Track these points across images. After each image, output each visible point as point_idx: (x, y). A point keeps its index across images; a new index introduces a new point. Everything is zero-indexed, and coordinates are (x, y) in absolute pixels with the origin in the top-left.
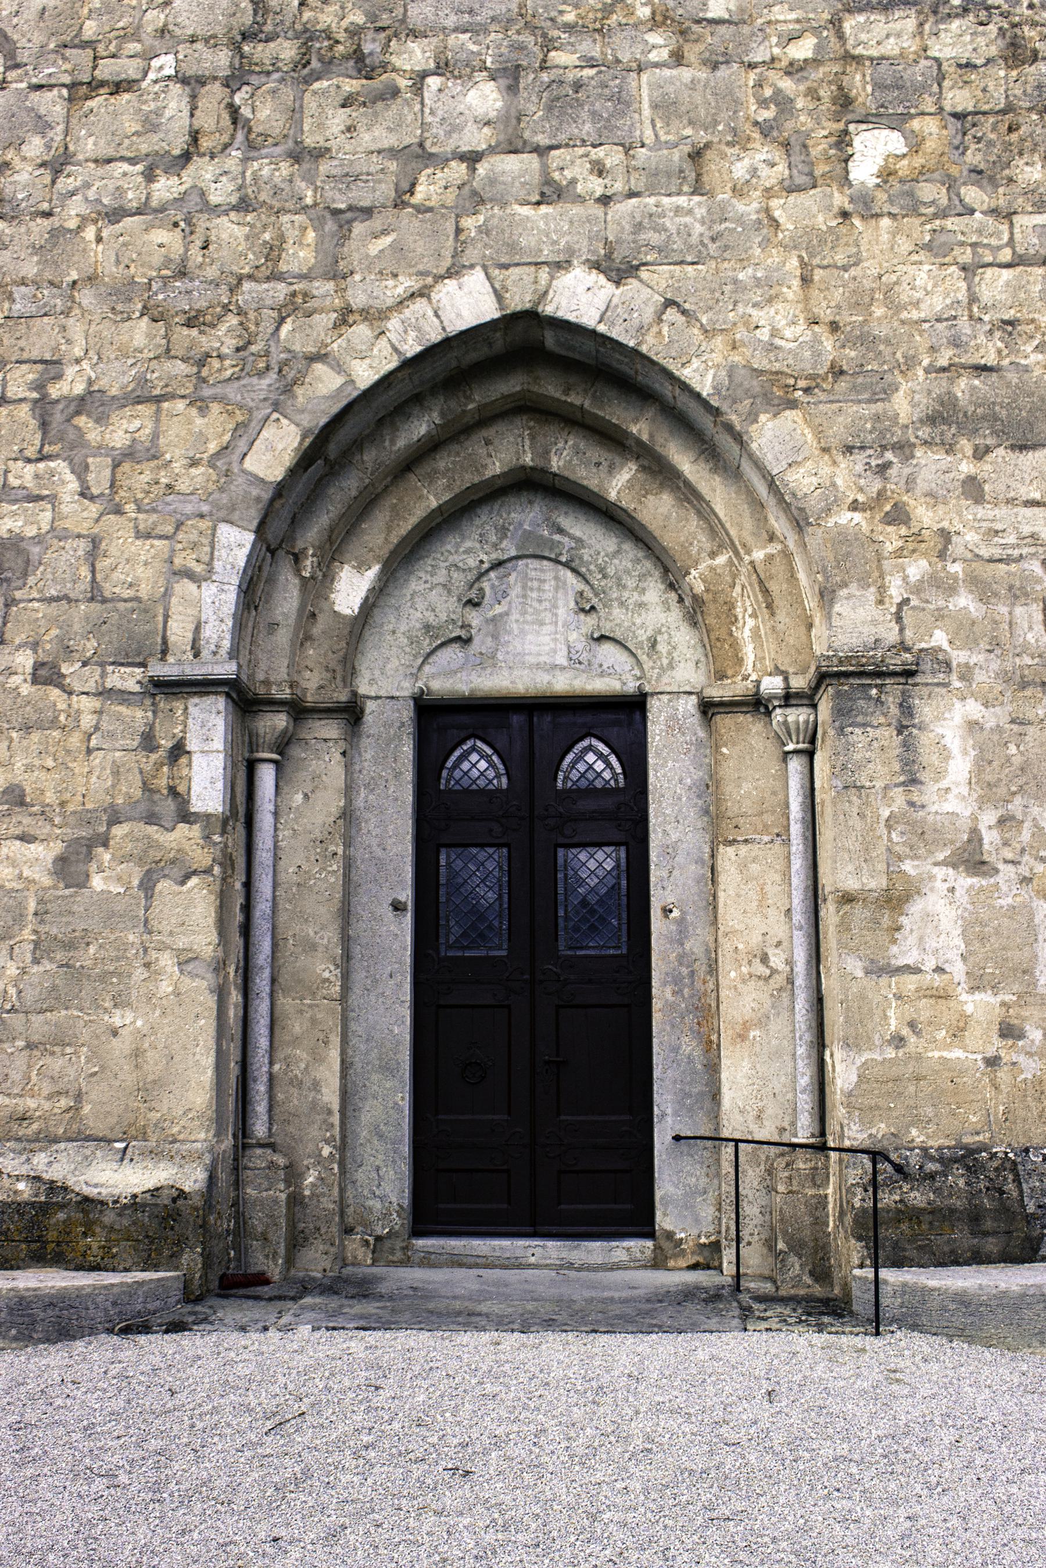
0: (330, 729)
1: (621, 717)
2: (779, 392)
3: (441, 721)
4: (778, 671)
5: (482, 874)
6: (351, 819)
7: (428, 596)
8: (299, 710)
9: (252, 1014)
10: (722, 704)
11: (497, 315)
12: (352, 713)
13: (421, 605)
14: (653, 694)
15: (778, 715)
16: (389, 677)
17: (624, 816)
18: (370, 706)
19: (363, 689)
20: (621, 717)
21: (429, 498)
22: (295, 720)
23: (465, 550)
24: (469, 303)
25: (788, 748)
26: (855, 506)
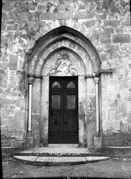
0: (38, 80)
1: (75, 79)
2: (97, 36)
3: (52, 79)
4: (94, 73)
5: (57, 99)
6: (42, 92)
7: (51, 63)
8: (35, 77)
9: (98, 101)
10: (88, 77)
11: (60, 26)
12: (41, 78)
13: (50, 64)
14: (79, 76)
15: (95, 78)
16: (46, 73)
17: (75, 92)
18: (44, 77)
19: (43, 75)
20: (75, 79)
21: (51, 50)
22: (99, 77)
23: (57, 56)
24: (56, 25)
25: (96, 82)
26: (105, 51)
